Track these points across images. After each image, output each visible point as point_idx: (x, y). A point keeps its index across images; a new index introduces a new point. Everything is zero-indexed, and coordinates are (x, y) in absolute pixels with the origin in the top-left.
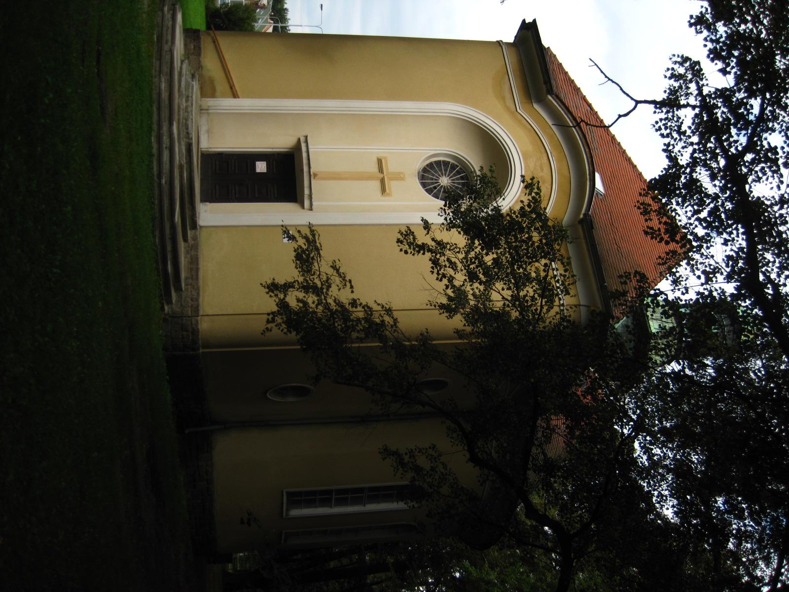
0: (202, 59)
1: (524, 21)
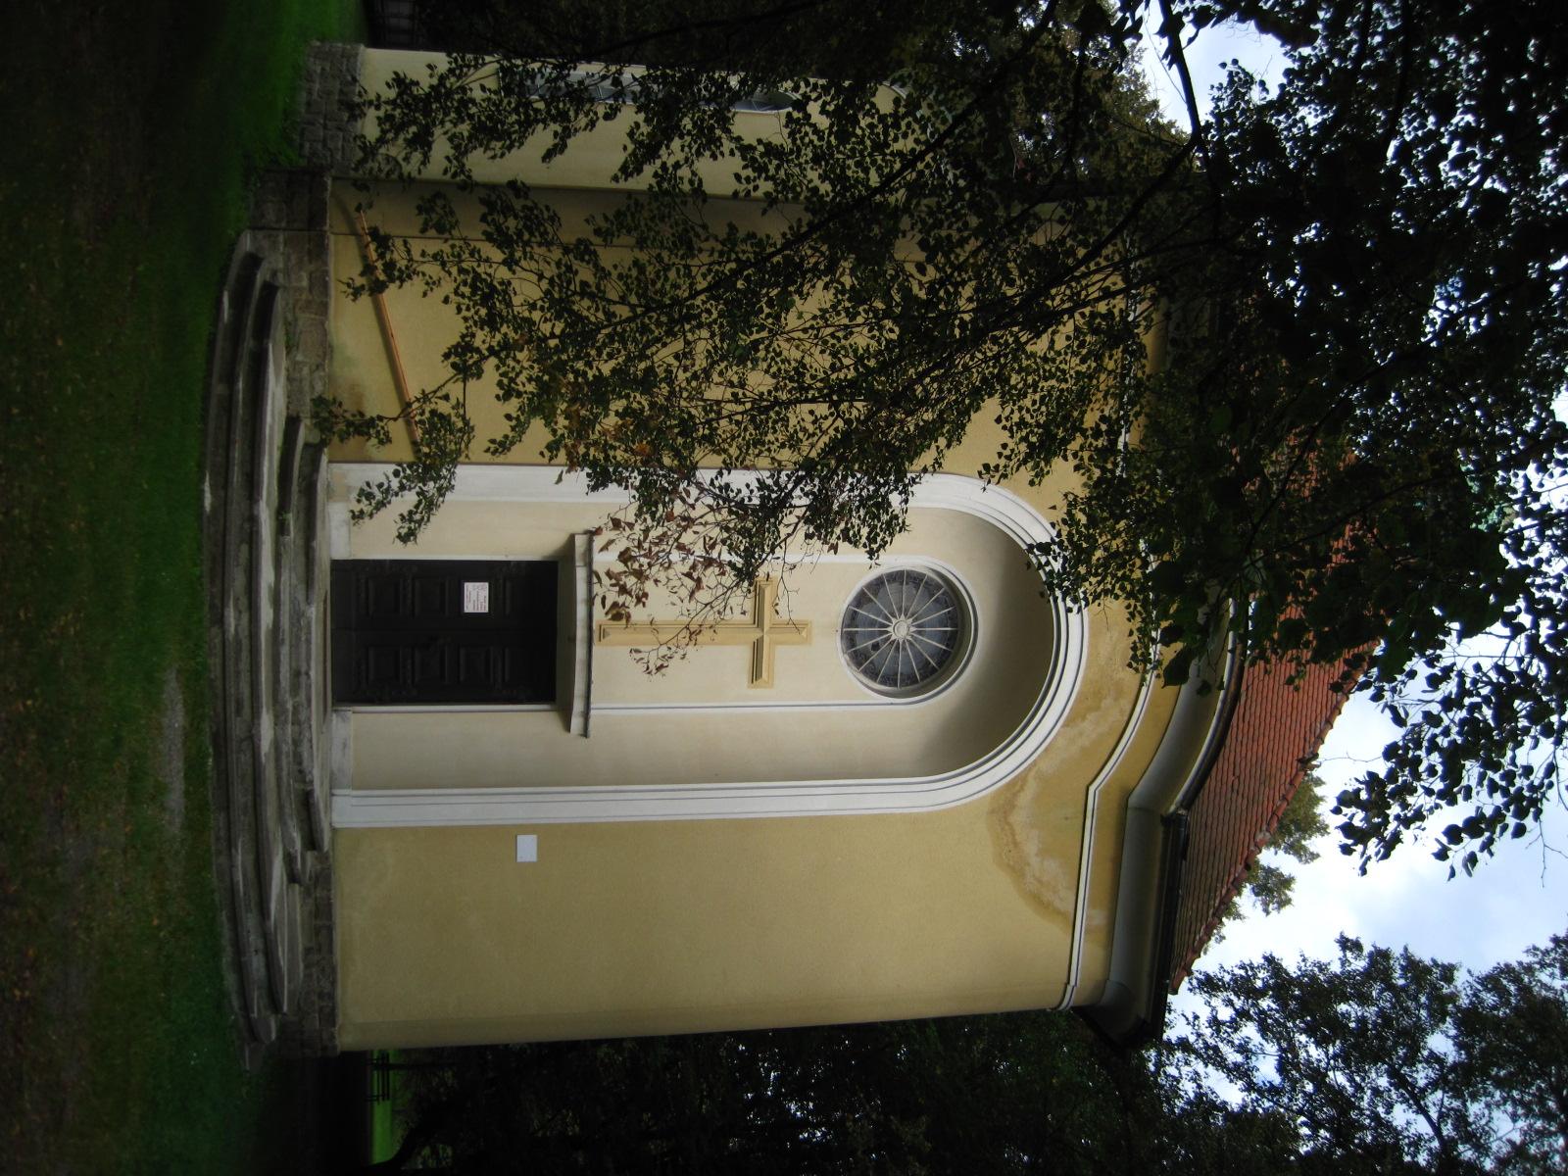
0: (332, 324)
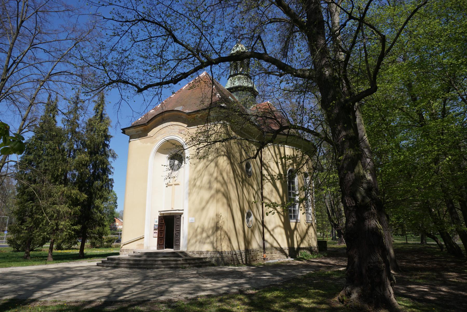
1: (122, 133)
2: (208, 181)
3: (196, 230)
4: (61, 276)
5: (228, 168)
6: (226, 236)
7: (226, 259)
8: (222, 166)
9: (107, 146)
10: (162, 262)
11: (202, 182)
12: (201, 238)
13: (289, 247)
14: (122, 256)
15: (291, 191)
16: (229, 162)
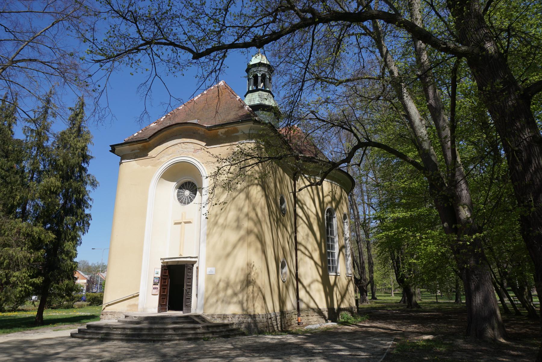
1: (110, 151)
2: (235, 218)
3: (218, 285)
4: (23, 358)
5: (263, 201)
6: (260, 294)
7: (260, 325)
8: (255, 198)
9: (85, 170)
10: (174, 331)
11: (226, 218)
12: (225, 296)
13: (328, 308)
14: (103, 321)
15: (329, 236)
16: (264, 193)
